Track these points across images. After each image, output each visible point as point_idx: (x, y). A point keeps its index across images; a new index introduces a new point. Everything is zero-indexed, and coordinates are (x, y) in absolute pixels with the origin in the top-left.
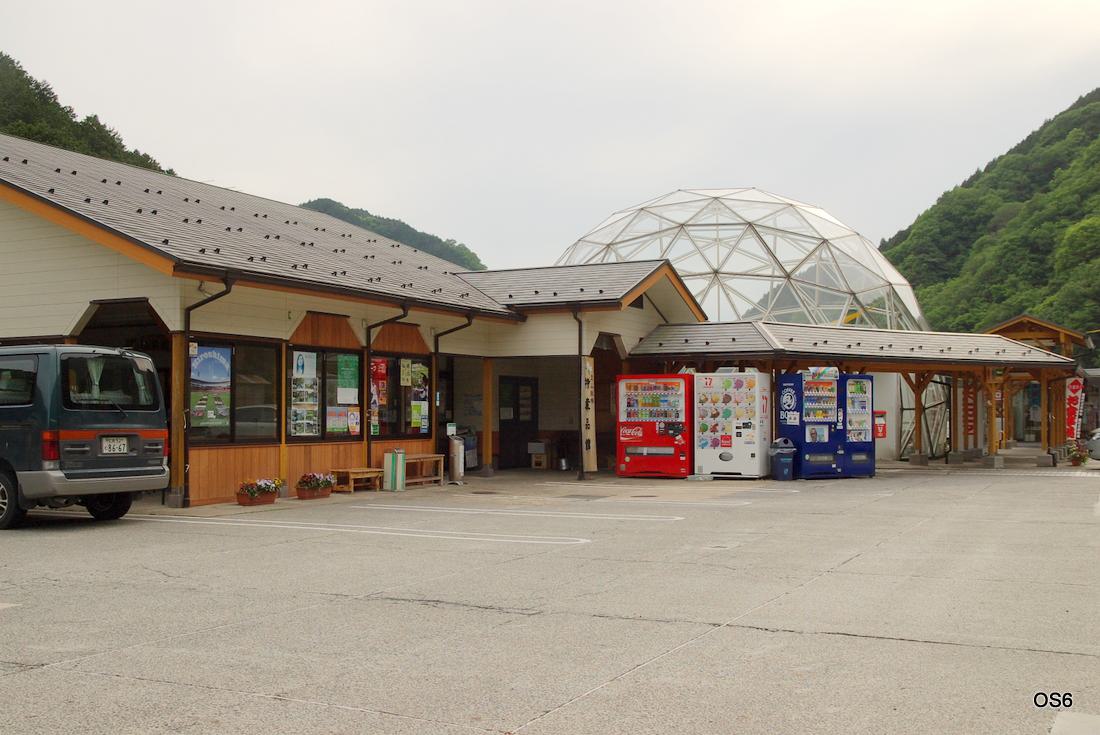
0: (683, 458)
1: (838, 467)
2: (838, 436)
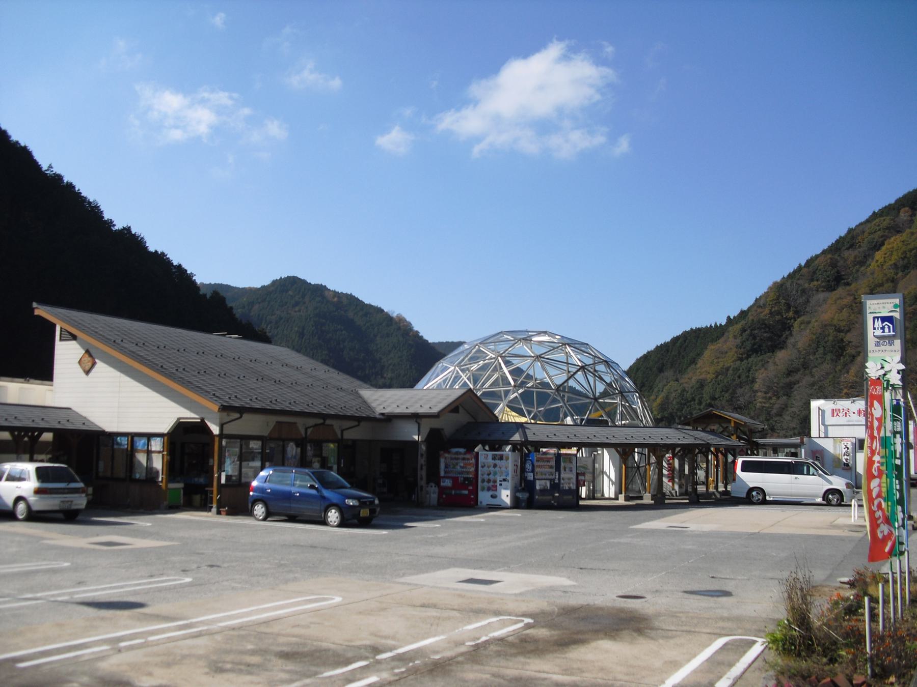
0: (472, 496)
1: (555, 502)
2: (555, 486)
